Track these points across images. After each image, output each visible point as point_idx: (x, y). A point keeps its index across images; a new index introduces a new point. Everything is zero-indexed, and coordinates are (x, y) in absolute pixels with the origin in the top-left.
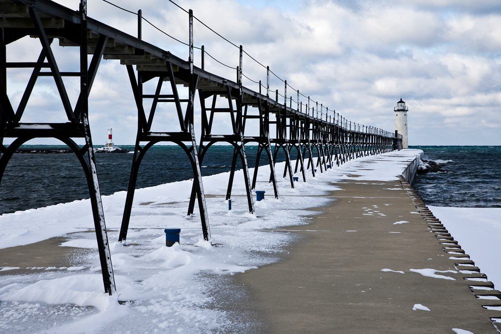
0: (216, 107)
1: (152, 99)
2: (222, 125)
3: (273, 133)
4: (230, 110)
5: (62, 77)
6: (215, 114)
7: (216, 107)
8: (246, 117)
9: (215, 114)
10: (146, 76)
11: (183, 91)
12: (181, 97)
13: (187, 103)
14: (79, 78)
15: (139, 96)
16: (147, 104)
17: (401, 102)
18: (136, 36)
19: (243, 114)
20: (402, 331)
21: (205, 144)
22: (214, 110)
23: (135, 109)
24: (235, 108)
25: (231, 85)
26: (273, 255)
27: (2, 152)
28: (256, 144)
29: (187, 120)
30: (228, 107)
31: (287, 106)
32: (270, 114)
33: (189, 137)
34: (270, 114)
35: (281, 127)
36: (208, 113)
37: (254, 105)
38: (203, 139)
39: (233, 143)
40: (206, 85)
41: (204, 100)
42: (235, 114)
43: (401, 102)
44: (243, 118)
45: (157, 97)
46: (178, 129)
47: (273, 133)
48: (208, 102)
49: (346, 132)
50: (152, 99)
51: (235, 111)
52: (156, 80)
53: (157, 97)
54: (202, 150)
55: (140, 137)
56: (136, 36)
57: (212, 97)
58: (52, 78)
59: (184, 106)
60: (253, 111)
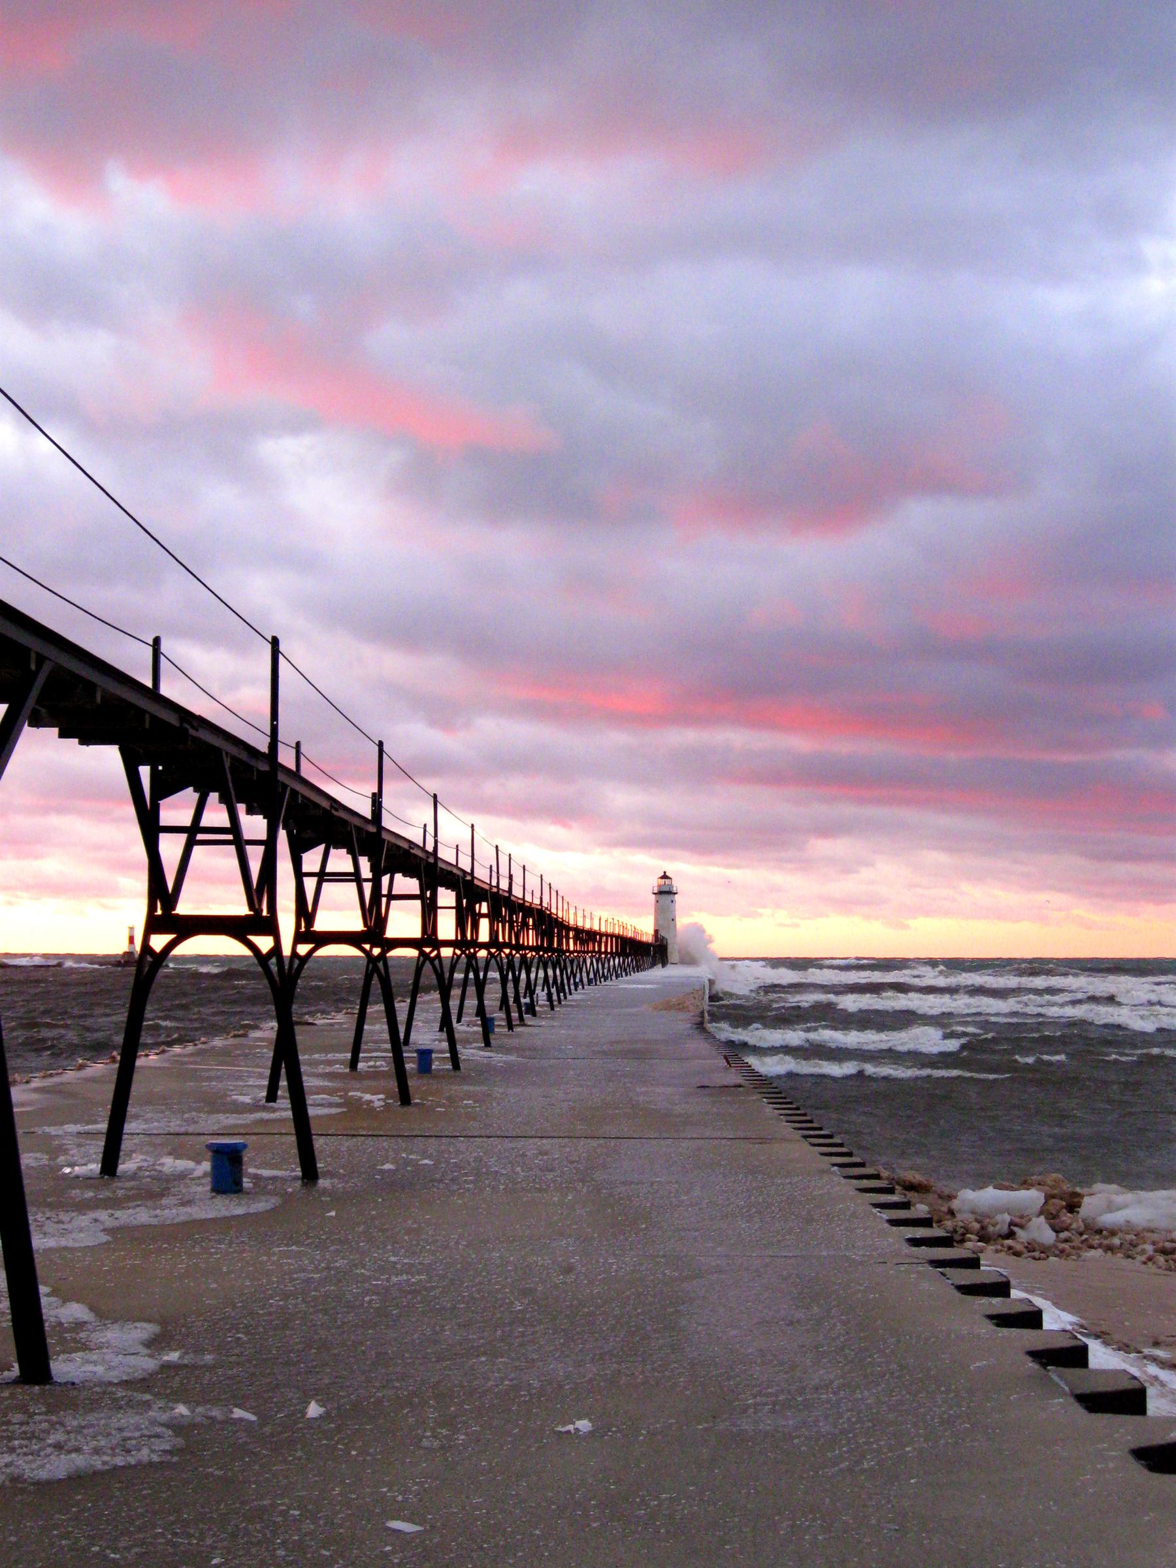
0: (328, 870)
1: (183, 837)
2: (340, 910)
3: (447, 927)
4: (356, 877)
5: (248, 847)
6: (393, 902)
7: (328, 870)
8: (391, 897)
9: (197, 850)
10: (164, 787)
11: (254, 825)
12: (247, 835)
13: (186, 835)
14: (163, 823)
15: (151, 829)
16: (170, 848)
17: (665, 877)
18: (293, 768)
19: (385, 891)
20: (683, 1234)
21: (303, 949)
22: (322, 876)
23: (139, 851)
24: (366, 873)
25: (357, 822)
26: (658, 983)
27: (377, 946)
28: (412, 953)
29: (261, 888)
30: (352, 870)
31: (514, 893)
32: (441, 891)
33: (270, 926)
34: (441, 891)
35: (465, 916)
36: (310, 884)
37: (407, 873)
38: (299, 938)
39: (363, 950)
40: (315, 821)
41: (301, 858)
42: (368, 888)
43: (665, 877)
44: (384, 900)
45: (193, 833)
46: (243, 910)
47: (447, 927)
48: (312, 860)
49: (568, 928)
50: (183, 837)
51: (367, 880)
52: (189, 796)
53: (193, 833)
54: (297, 962)
55: (154, 925)
56: (293, 768)
57: (322, 847)
58: (232, 848)
59: (255, 856)
60: (406, 884)
